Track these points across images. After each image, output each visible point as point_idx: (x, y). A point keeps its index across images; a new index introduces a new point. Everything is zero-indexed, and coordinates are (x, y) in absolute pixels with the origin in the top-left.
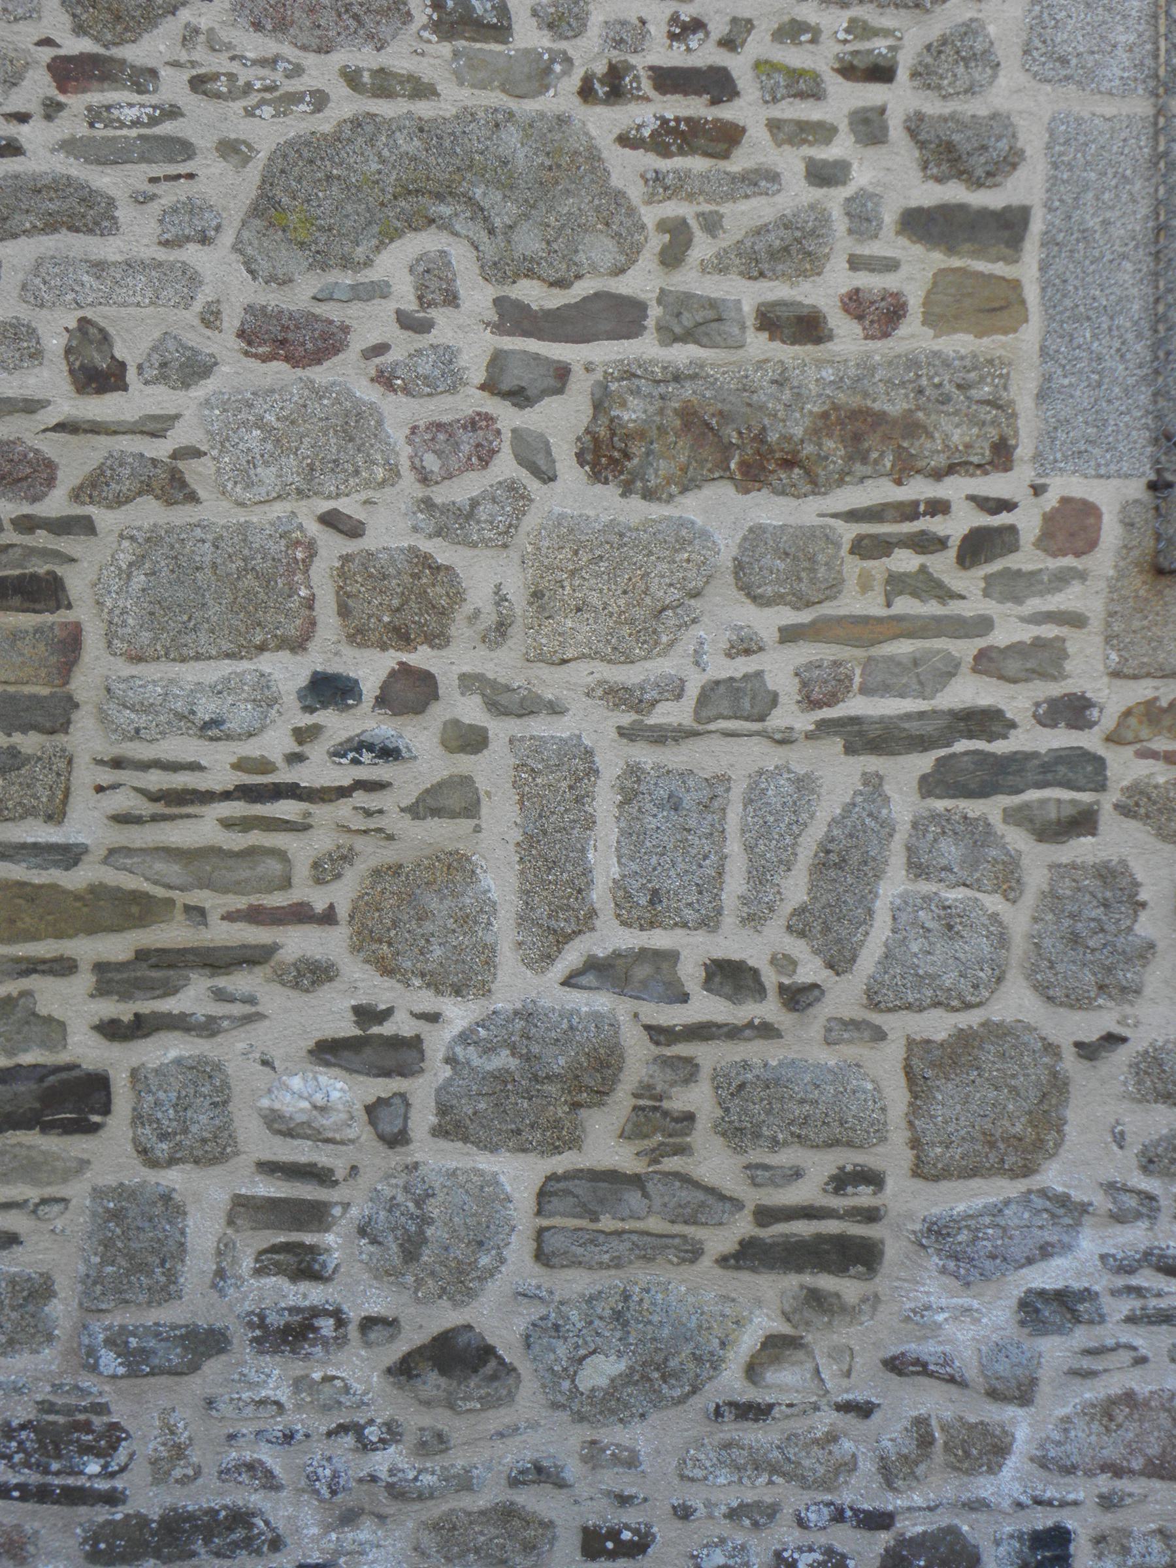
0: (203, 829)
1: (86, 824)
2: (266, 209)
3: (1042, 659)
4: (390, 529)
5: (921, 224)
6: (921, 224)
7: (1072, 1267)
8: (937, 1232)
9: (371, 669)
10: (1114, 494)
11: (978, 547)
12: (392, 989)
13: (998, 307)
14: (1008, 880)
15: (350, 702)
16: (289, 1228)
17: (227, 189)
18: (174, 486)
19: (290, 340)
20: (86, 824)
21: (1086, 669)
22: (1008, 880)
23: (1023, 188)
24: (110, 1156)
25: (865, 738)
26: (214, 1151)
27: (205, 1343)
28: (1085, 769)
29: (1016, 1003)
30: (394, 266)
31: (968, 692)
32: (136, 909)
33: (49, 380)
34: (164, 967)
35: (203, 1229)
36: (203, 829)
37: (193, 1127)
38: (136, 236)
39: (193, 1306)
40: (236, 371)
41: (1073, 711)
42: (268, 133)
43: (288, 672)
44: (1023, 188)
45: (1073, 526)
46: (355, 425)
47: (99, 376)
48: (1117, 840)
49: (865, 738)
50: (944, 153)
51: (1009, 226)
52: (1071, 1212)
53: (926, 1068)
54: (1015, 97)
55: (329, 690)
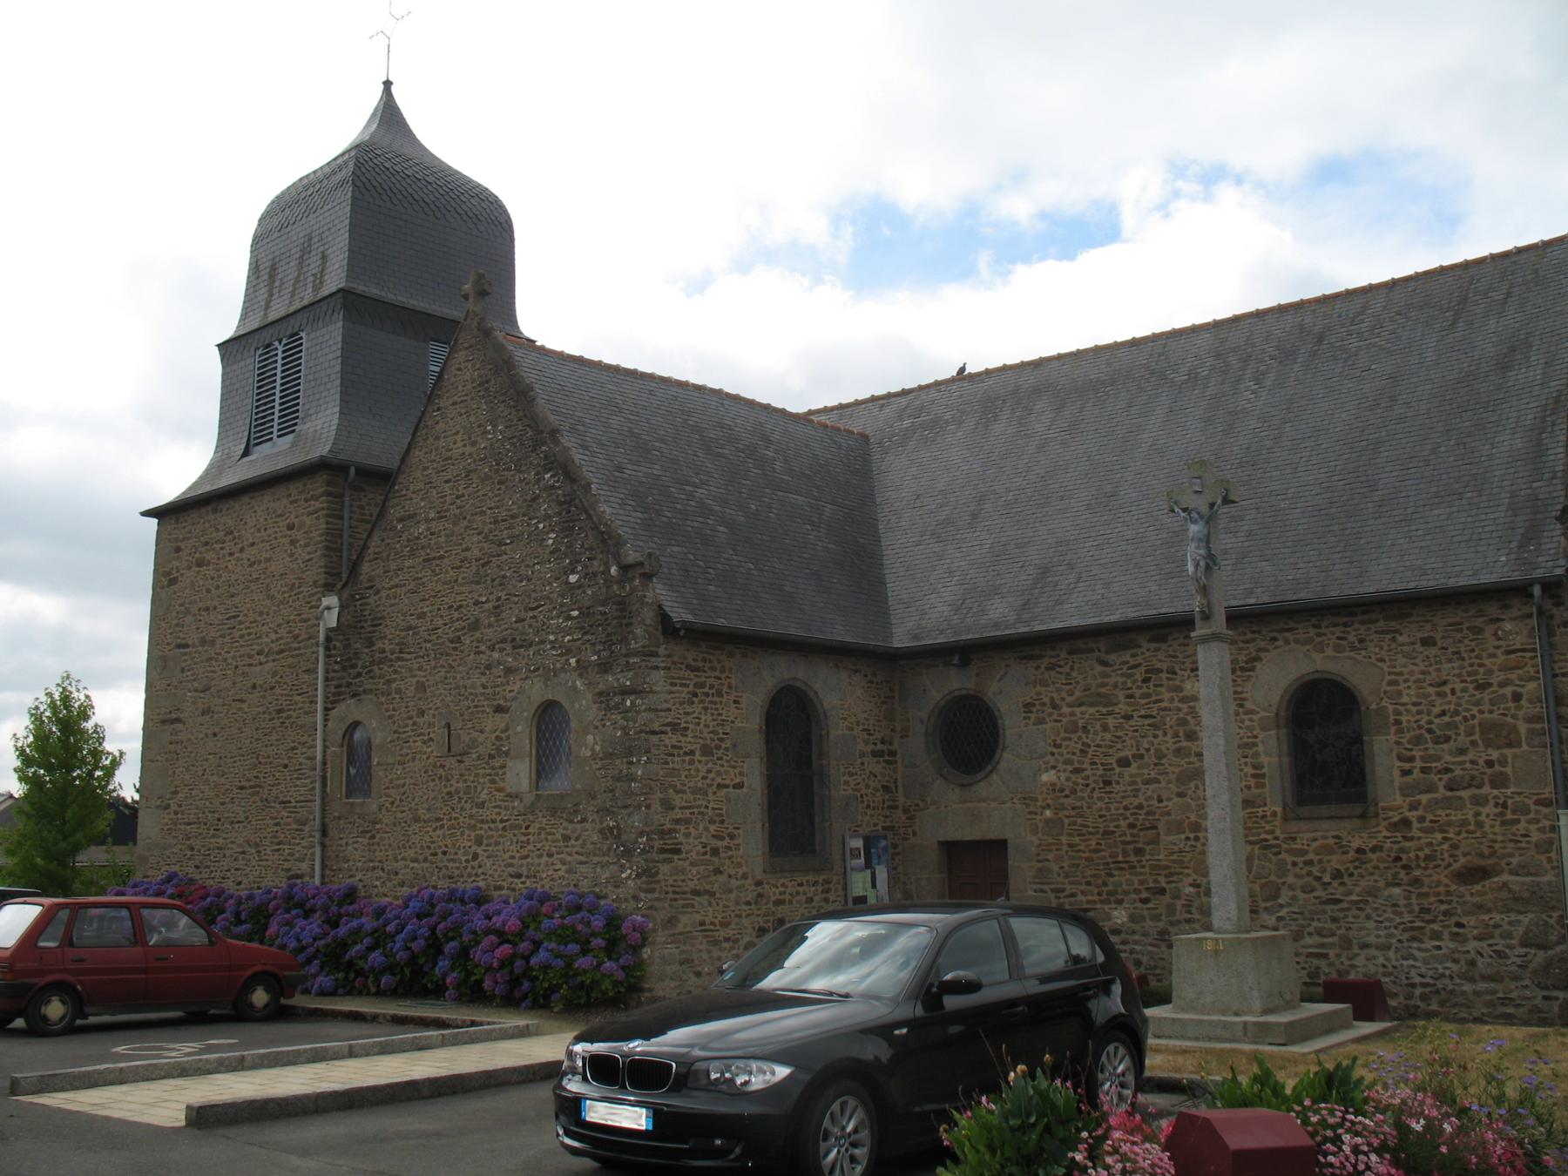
0: (1174, 857)
1: (1162, 857)
2: (1178, 779)
3: (1272, 832)
4: (1193, 818)
5: (1254, 776)
6: (1254, 776)
7: (1283, 913)
8: (1266, 909)
9: (1192, 836)
10: (1279, 809)
11: (1263, 817)
12: (1250, 592)
13: (1263, 786)
14: (1270, 861)
15: (184, 929)
16: (1187, 907)
17: (1172, 777)
18: (1169, 813)
19: (1181, 795)
20: (1162, 857)
21: (1278, 833)
22: (1270, 861)
23: (1265, 770)
24: (1167, 899)
25: (1252, 843)
26: (1179, 898)
27: (1179, 922)
28: (1279, 846)
29: (1273, 878)
30: (1192, 785)
31: (1264, 836)
32: (1167, 867)
33: (1155, 802)
34: (1172, 874)
35: (1179, 908)
36: (1174, 857)
37: (1177, 897)
38: (1163, 784)
39: (1178, 917)
40: (1176, 800)
41: (1276, 838)
42: (1177, 770)
43: (1183, 836)
44: (1265, 770)
45: (1274, 814)
46: (1188, 805)
47: (1160, 801)
48: (1284, 856)
49: (1252, 843)
50: (1254, 767)
51: (1263, 776)
52: (1281, 906)
53: (1263, 886)
54: (1264, 759)
55: (1188, 839)
